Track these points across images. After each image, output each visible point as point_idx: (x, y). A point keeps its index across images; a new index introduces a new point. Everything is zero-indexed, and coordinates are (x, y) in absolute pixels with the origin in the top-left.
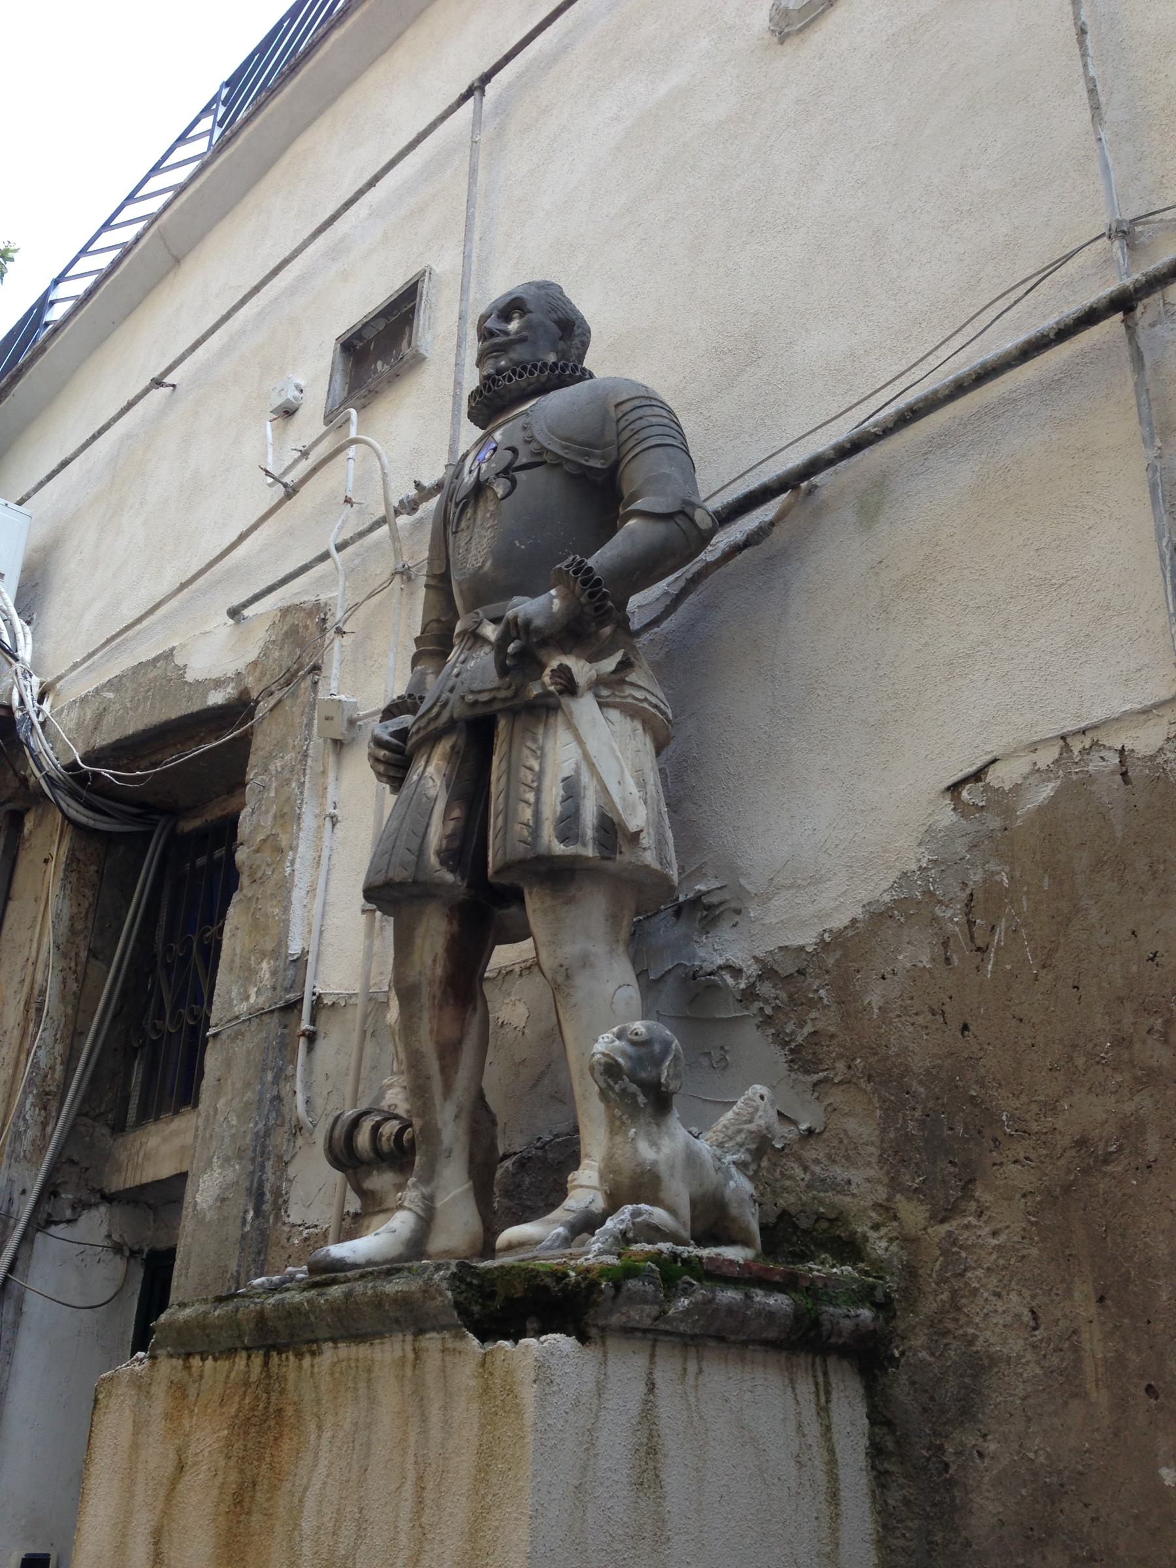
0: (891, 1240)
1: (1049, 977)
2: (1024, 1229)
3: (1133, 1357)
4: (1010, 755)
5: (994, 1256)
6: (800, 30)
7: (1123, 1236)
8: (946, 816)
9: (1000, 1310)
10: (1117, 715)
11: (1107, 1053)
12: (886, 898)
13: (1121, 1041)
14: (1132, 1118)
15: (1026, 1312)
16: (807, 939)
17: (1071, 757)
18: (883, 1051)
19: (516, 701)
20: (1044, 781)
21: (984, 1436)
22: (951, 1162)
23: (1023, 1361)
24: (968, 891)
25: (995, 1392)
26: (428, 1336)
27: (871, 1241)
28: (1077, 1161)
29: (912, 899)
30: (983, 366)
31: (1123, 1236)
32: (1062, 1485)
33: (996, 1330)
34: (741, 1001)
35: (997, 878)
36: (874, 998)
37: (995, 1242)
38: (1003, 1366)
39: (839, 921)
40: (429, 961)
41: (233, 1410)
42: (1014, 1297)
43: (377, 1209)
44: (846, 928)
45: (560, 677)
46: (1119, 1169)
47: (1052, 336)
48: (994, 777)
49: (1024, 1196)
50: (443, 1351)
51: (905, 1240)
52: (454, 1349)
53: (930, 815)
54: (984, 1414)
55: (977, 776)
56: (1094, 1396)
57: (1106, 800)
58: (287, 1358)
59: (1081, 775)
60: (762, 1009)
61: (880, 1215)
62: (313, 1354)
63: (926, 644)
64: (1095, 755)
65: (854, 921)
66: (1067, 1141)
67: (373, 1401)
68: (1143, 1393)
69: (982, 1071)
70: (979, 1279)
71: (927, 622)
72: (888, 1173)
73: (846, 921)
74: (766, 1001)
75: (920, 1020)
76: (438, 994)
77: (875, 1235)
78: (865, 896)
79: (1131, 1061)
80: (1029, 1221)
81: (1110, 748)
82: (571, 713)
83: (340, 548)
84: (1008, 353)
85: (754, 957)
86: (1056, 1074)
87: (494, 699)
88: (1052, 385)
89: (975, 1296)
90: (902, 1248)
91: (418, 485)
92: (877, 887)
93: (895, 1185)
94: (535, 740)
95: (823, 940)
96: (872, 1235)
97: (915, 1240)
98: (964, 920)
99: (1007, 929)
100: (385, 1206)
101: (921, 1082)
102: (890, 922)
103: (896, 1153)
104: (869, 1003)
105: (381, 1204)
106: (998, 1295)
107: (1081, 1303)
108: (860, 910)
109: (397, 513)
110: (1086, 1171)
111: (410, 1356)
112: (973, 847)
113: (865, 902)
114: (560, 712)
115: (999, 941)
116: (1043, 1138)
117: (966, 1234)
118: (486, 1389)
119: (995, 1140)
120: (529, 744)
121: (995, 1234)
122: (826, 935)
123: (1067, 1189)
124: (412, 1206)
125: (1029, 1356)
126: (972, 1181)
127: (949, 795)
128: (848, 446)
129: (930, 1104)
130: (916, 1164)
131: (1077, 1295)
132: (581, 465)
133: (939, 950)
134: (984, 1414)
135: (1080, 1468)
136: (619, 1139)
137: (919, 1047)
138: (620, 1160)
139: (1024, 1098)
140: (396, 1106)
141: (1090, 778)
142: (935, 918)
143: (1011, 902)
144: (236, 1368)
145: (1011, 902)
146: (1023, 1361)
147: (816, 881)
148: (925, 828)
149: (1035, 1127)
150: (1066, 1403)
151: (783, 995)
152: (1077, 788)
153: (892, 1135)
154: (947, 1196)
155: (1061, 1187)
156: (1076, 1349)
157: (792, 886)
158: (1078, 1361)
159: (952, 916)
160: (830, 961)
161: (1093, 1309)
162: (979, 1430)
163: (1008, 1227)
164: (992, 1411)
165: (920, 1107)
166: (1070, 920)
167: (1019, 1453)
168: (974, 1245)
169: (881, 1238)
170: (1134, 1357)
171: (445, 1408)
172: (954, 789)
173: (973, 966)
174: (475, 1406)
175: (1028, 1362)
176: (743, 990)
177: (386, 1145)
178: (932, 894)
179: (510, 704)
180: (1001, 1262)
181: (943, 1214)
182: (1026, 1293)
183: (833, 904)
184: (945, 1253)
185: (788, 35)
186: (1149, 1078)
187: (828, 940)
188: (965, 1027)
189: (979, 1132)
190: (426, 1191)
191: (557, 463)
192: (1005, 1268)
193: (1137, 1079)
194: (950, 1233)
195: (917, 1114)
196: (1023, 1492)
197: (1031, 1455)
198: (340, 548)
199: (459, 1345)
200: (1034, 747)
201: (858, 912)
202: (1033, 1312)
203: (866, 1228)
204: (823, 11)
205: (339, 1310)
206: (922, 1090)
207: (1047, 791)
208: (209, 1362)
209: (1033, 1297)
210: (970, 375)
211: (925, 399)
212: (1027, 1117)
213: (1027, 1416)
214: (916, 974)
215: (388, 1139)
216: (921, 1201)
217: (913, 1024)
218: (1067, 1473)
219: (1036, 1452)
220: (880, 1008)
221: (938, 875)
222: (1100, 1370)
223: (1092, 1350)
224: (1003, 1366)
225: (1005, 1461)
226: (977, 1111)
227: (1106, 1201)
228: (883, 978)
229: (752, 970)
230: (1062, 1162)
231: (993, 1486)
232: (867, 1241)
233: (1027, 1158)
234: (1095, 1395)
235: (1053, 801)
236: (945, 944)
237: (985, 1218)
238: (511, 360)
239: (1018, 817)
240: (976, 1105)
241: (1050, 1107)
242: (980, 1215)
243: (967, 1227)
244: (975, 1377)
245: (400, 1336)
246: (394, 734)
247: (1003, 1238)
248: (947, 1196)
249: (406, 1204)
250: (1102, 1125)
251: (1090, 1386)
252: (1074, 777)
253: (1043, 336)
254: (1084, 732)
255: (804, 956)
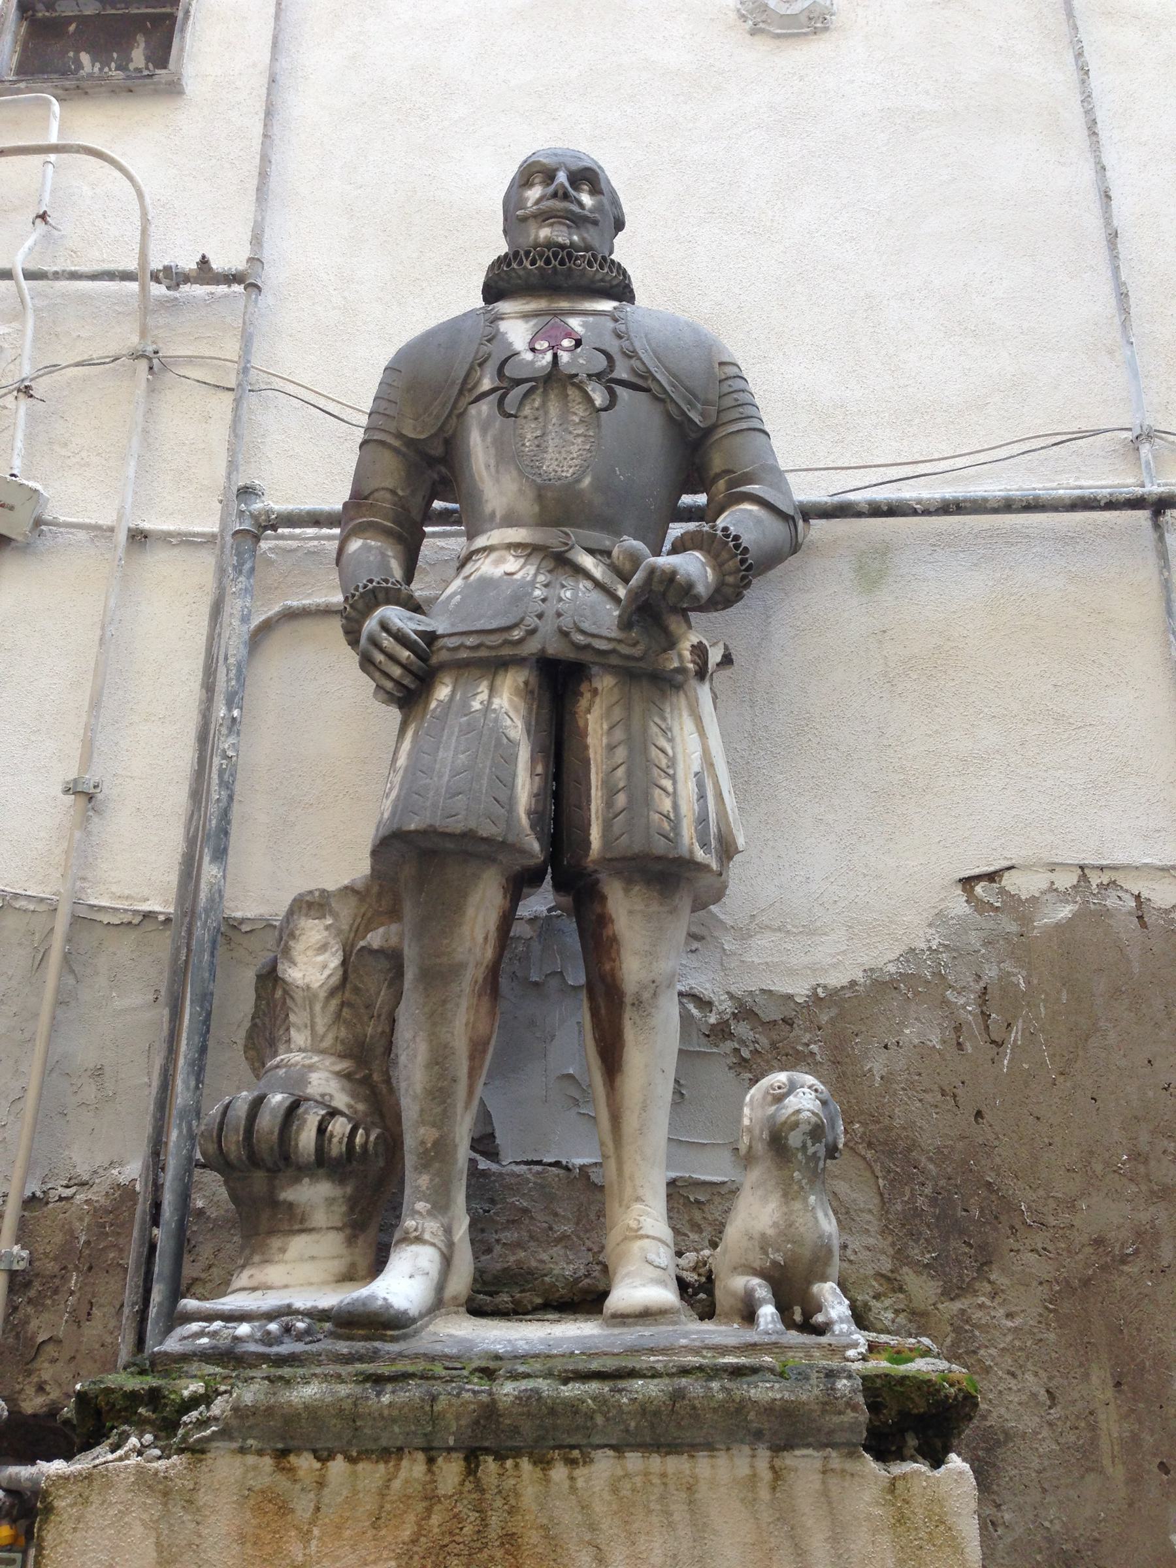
0: (897, 1312)
1: (1068, 1084)
2: (1040, 1315)
3: (1148, 1440)
4: (1028, 868)
5: (1009, 1338)
6: (778, 36)
7: (1138, 1330)
8: (959, 905)
9: (1015, 1388)
10: (1138, 864)
11: (1123, 1164)
12: (892, 968)
13: (1137, 1156)
14: (1148, 1227)
15: (1043, 1392)
16: (799, 989)
17: (1089, 887)
18: (887, 1121)
19: (641, 664)
20: (1061, 901)
21: (998, 1506)
22: (965, 1242)
23: (1040, 1437)
24: (982, 984)
25: (1010, 1464)
26: (797, 1453)
27: (875, 1310)
28: (1093, 1258)
29: (920, 977)
30: (1036, 498)
31: (1138, 1330)
32: (1078, 1551)
33: (1011, 1406)
34: (708, 1036)
35: (1013, 979)
36: (877, 1065)
37: (1010, 1324)
38: (1018, 1441)
39: (837, 979)
40: (480, 939)
41: (406, 1533)
42: (1029, 1377)
43: (296, 1227)
44: (843, 987)
45: (699, 656)
46: (1136, 1270)
47: (1102, 504)
48: (1009, 881)
49: (1041, 1283)
50: (824, 1472)
51: (913, 1313)
52: (843, 1471)
53: (942, 900)
54: (998, 1485)
55: (991, 877)
56: (1110, 1470)
57: (1124, 936)
58: (517, 1466)
59: (1097, 907)
60: (736, 1050)
61: (881, 1285)
62: (572, 1463)
63: (937, 732)
64: (1112, 893)
65: (853, 983)
66: (1085, 1239)
67: (700, 1527)
68: (1156, 1470)
69: (998, 1160)
70: (993, 1358)
71: (937, 710)
72: (893, 1244)
73: (844, 982)
74: (743, 1042)
75: (928, 1097)
76: (480, 980)
77: (879, 1305)
78: (868, 961)
79: (1147, 1175)
80: (1047, 1308)
81: (1127, 891)
82: (697, 700)
83: (30, 276)
84: (1061, 499)
85: (728, 993)
86: (1074, 1175)
87: (614, 651)
88: (1067, 540)
89: (988, 1372)
90: (910, 1321)
91: (204, 262)
92: (883, 955)
93: (901, 1257)
94: (664, 719)
95: (815, 994)
96: (873, 1303)
97: (924, 1314)
98: (978, 1011)
99: (1023, 1030)
100: (307, 1225)
101: (930, 1159)
102: (894, 994)
103: (903, 1225)
104: (870, 1070)
105: (302, 1221)
106: (1013, 1375)
107: (1098, 1385)
108: (861, 974)
109: (155, 277)
110: (1104, 1268)
111: (767, 1475)
112: (987, 943)
113: (867, 967)
114: (681, 693)
115: (1015, 1040)
116: (1060, 1232)
117: (979, 1314)
118: (901, 1520)
119: (1012, 1227)
120: (657, 720)
121: (1010, 1315)
122: (820, 990)
123: (1086, 1282)
124: (436, 1241)
125: (1045, 1432)
126: (988, 1263)
127: (960, 886)
128: (885, 508)
129: (942, 1183)
130: (926, 1240)
131: (1094, 1380)
132: (684, 413)
133: (950, 1034)
134: (998, 1485)
135: (1096, 1534)
136: (797, 1205)
137: (931, 1126)
138: (802, 1229)
139: (1041, 1192)
140: (331, 1096)
141: (1106, 913)
142: (945, 1002)
143: (1028, 1004)
144: (403, 1474)
145: (1028, 1004)
146: (1040, 1437)
147: (811, 931)
148: (937, 911)
149: (1052, 1221)
150: (1082, 1477)
151: (764, 1041)
152: (1093, 917)
153: (899, 1207)
154: (960, 1276)
155: (1079, 1280)
156: (1093, 1428)
157: (779, 929)
158: (1094, 1441)
159: (966, 1005)
160: (824, 1018)
161: (1110, 1393)
162: (994, 1501)
163: (1023, 1311)
164: (1007, 1483)
165: (930, 1184)
166: (1088, 1037)
167: (1034, 1522)
168: (987, 1325)
169: (886, 1309)
170: (1148, 1437)
171: (834, 1539)
172: (968, 883)
173: (989, 1057)
174: (885, 1540)
175: (1044, 1439)
176: (713, 1025)
177: (336, 1148)
178: (943, 977)
179: (632, 664)
180: (1017, 1343)
181: (950, 1293)
182: (1042, 1373)
183: (829, 960)
184: (958, 1330)
185: (762, 31)
186: (1162, 1194)
187: (822, 995)
188: (979, 1114)
189: (996, 1218)
190: (445, 1221)
191: (661, 398)
192: (1021, 1349)
193: (1152, 1192)
194: (963, 1311)
195: (928, 1190)
196: (1039, 1557)
197: (1047, 1524)
198: (30, 276)
199: (849, 1465)
200: (1052, 868)
201: (859, 976)
202: (1048, 1391)
203: (867, 1297)
204: (805, 34)
205: (657, 1413)
206: (931, 1167)
207: (1065, 912)
208: (338, 1466)
209: (1050, 1378)
210: (1021, 500)
211: (974, 501)
212: (1045, 1210)
213: (1043, 1488)
214: (923, 1051)
215: (340, 1142)
216: (933, 1277)
217: (920, 1100)
218: (1082, 1540)
219: (1051, 1522)
220: (882, 1078)
221: (950, 961)
222: (1116, 1447)
223: (1109, 1430)
224: (1018, 1441)
225: (1019, 1530)
226: (993, 1197)
227: (1123, 1298)
228: (886, 1047)
229: (727, 1006)
230: (1080, 1256)
231: (1008, 1553)
232: (870, 1310)
233: (1045, 1249)
234: (1111, 1470)
235: (1071, 921)
236: (958, 1029)
237: (998, 1300)
238: (584, 239)
239: (1035, 928)
240: (992, 1191)
241: (1071, 1205)
242: (993, 1296)
243: (981, 1306)
244: (988, 1450)
245: (746, 1449)
246: (422, 634)
247: (1018, 1321)
248: (960, 1276)
249: (427, 1236)
250: (1118, 1228)
251: (1106, 1462)
252: (1092, 906)
253: (1095, 499)
254: (1102, 868)
255: (792, 1005)
